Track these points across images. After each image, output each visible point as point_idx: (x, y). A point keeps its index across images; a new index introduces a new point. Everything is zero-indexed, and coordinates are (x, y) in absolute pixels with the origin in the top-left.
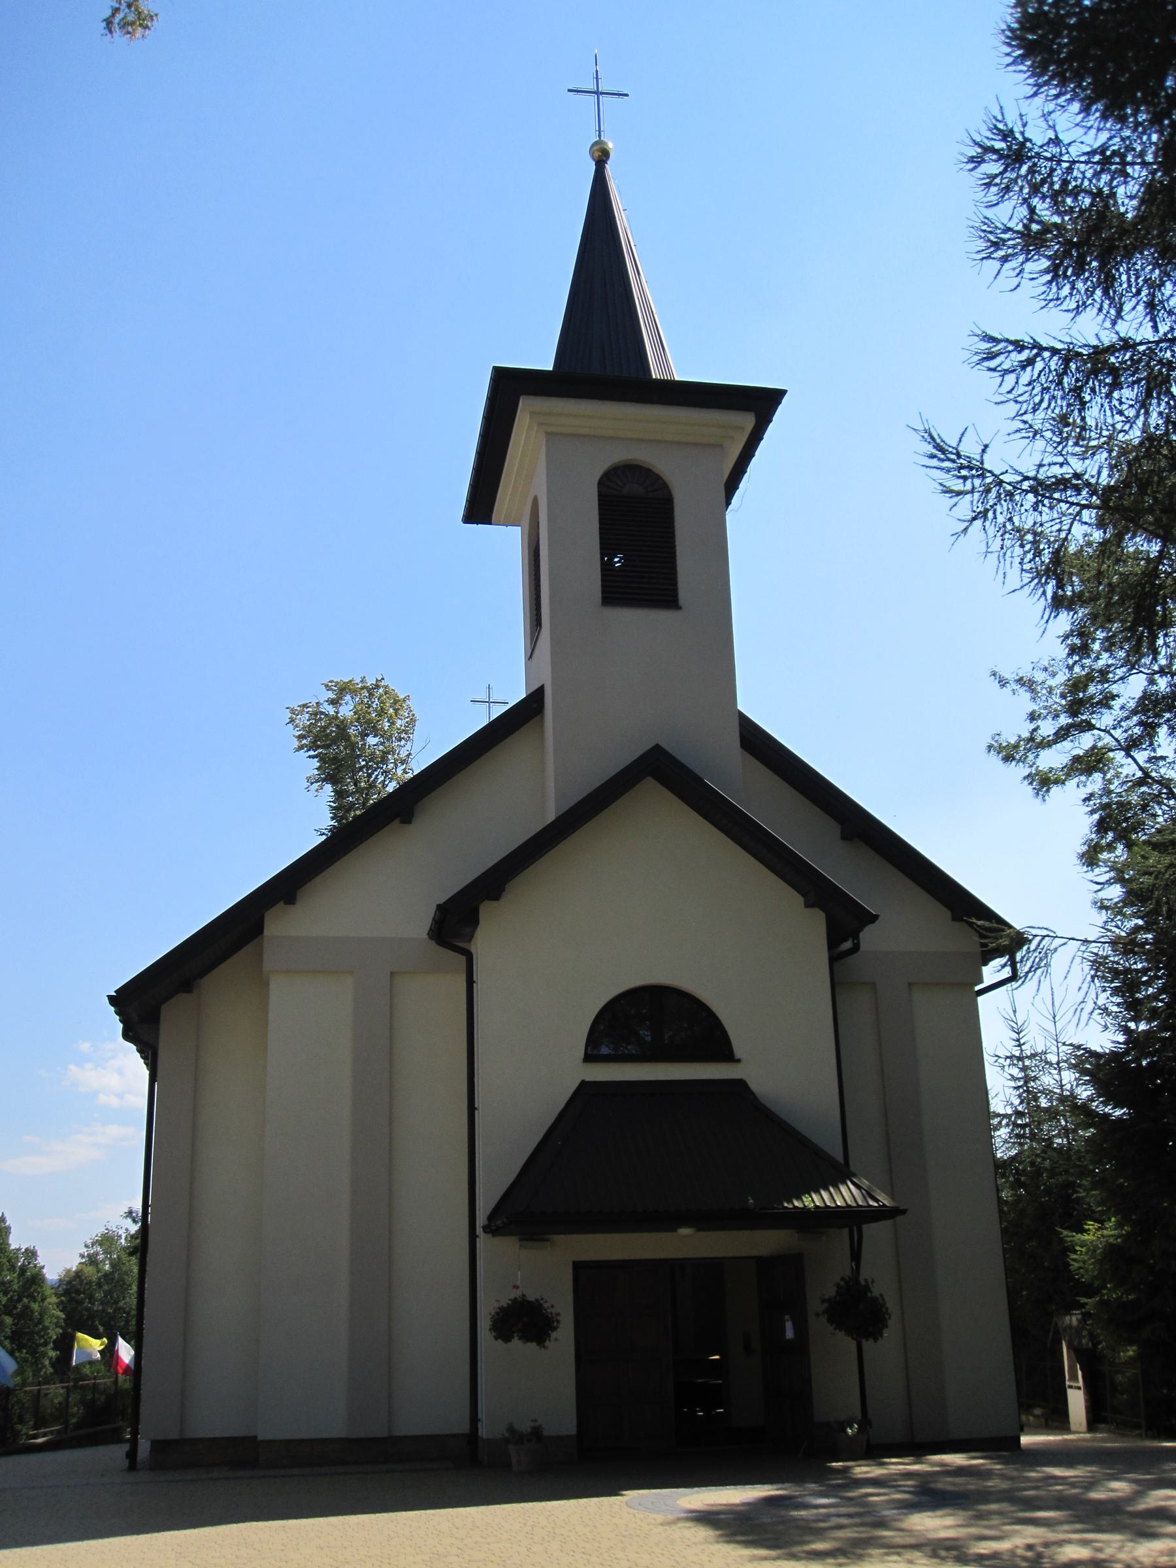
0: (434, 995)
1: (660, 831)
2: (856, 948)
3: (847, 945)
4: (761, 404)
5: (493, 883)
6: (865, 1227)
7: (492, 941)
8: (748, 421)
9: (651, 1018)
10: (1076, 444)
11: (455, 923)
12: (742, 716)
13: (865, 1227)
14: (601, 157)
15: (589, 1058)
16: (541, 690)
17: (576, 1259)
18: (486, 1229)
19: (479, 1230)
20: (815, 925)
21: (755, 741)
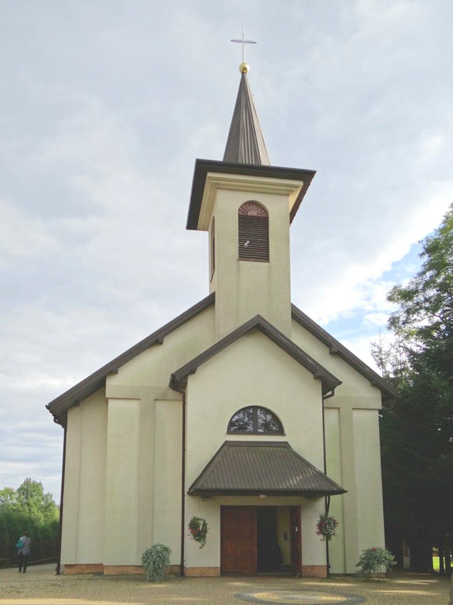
0: (168, 411)
1: (252, 356)
2: (333, 395)
3: (330, 393)
4: (306, 176)
5: (191, 368)
6: (331, 497)
7: (194, 385)
8: (301, 184)
9: (254, 419)
10: (23, 495)
11: (178, 383)
12: (293, 308)
13: (331, 497)
14: (244, 71)
15: (229, 432)
16: (214, 293)
17: (222, 504)
18: (189, 493)
19: (186, 494)
20: (319, 387)
21: (298, 318)
